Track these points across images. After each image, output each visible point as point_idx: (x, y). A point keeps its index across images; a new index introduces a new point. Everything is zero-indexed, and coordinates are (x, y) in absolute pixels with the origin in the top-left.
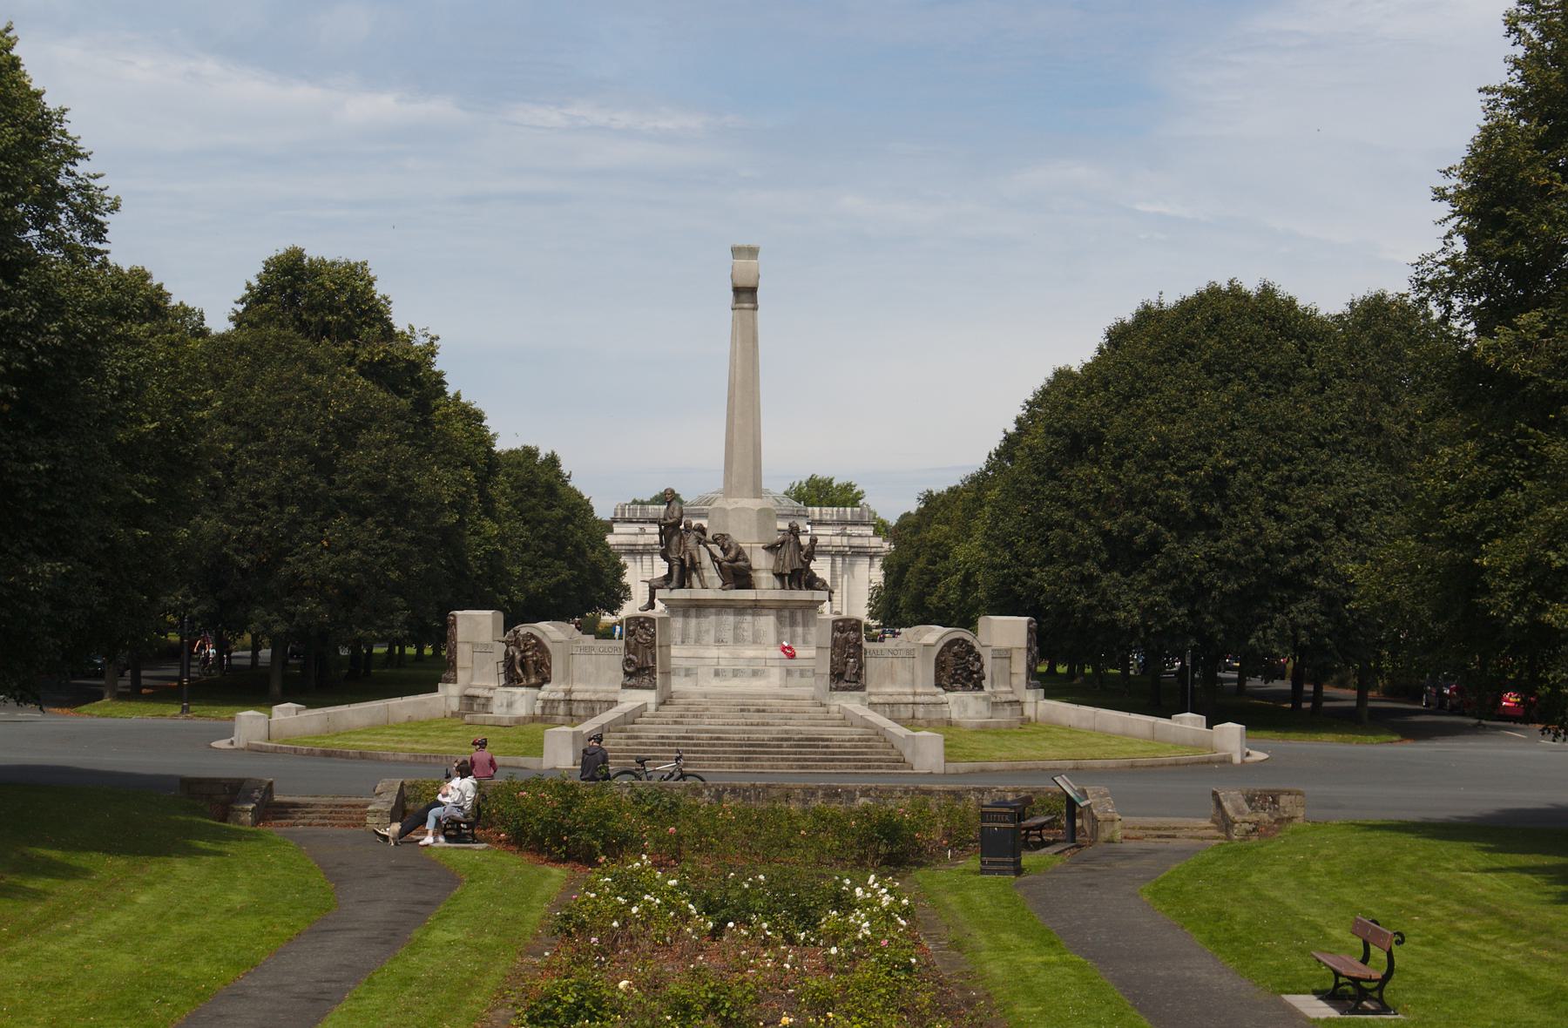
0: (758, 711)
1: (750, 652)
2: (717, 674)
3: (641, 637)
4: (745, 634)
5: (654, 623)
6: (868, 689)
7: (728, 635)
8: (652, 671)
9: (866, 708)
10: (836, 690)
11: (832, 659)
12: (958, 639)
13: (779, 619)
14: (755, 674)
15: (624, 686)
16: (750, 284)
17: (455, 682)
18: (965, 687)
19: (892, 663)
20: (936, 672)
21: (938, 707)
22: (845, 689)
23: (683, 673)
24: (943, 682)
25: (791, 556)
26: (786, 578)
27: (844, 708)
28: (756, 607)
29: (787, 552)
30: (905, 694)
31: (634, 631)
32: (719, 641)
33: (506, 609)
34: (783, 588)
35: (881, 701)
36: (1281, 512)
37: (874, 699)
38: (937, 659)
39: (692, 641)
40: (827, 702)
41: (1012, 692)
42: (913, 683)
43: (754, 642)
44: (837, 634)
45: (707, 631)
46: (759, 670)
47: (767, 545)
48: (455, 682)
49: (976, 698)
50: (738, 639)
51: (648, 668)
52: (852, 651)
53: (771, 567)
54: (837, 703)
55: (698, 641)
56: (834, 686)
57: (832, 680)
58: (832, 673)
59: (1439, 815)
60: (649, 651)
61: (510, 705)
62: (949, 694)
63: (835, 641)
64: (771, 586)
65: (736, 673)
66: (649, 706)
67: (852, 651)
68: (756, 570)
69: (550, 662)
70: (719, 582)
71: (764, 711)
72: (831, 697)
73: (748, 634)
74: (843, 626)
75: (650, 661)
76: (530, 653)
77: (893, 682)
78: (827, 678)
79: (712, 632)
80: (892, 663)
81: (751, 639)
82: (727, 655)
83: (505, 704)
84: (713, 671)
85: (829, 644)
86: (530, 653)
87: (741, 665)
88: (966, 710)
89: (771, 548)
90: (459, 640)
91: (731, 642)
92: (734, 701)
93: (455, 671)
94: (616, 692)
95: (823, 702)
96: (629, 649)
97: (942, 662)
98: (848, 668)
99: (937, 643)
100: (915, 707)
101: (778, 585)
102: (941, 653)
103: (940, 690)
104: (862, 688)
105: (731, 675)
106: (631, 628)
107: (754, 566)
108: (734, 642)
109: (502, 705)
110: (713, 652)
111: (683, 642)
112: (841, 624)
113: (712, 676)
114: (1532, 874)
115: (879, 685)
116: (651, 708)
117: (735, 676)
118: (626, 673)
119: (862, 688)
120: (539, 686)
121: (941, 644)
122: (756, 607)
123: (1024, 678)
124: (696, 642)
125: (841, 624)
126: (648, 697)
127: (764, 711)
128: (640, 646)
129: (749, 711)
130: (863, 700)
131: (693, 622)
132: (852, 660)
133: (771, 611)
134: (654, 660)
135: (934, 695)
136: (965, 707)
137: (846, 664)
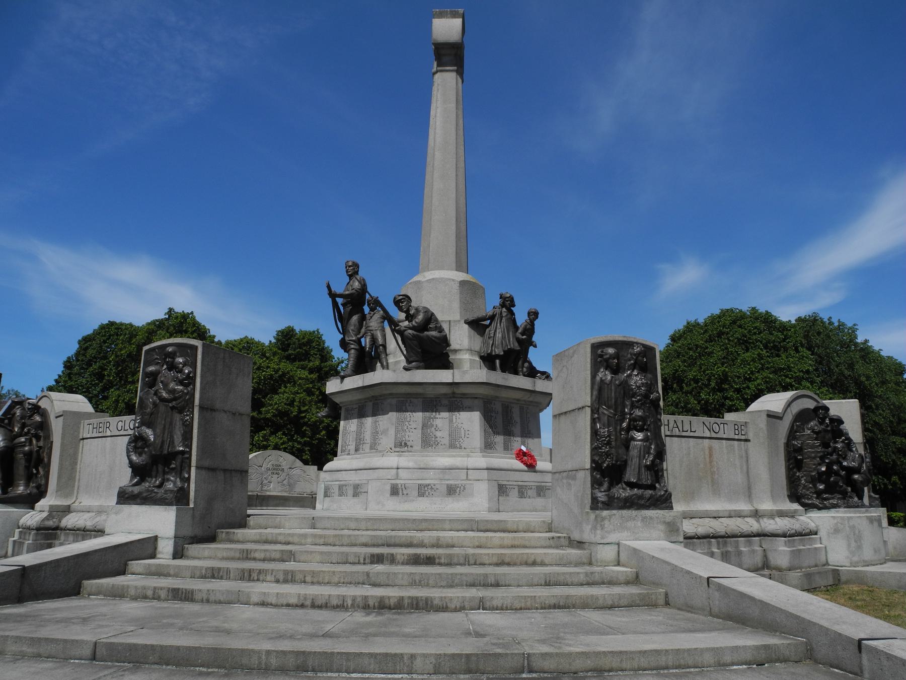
0: (416, 560)
1: (444, 460)
3: (166, 385)
4: (438, 434)
6: (679, 507)
7: (414, 436)
9: (680, 548)
10: (609, 504)
11: (595, 433)
13: (488, 417)
14: (451, 491)
15: (125, 497)
19: (710, 449)
20: (789, 470)
22: (628, 504)
23: (350, 491)
24: (801, 491)
25: (503, 333)
26: (498, 362)
27: (635, 551)
29: (499, 331)
30: (739, 515)
32: (401, 445)
35: (701, 531)
37: (689, 527)
38: (788, 445)
39: (367, 447)
40: (587, 536)
42: (749, 493)
43: (452, 446)
44: (606, 375)
45: (385, 432)
46: (457, 486)
47: (471, 319)
50: (428, 442)
51: (174, 455)
52: (638, 413)
54: (613, 537)
55: (373, 447)
56: (601, 496)
57: (596, 483)
58: (596, 467)
60: (177, 417)
62: (815, 515)
63: (600, 391)
65: (423, 491)
67: (638, 413)
68: (456, 351)
70: (403, 362)
71: (430, 561)
72: (599, 523)
73: (443, 435)
74: (617, 356)
77: (716, 490)
78: (584, 478)
79: (392, 432)
80: (710, 449)
81: (446, 441)
82: (411, 465)
84: (388, 487)
85: (586, 398)
86: (23, 439)
87: (431, 478)
88: (859, 547)
89: (477, 325)
91: (418, 445)
92: (365, 535)
94: (100, 511)
95: (576, 536)
98: (634, 452)
100: (767, 543)
103: (796, 506)
104: (664, 502)
105: (416, 493)
106: (151, 368)
110: (392, 460)
111: (357, 450)
112: (611, 351)
113: (388, 494)
115: (691, 496)
117: (421, 494)
119: (664, 502)
124: (371, 448)
125: (611, 351)
127: (430, 561)
128: (162, 408)
129: (392, 560)
130: (672, 529)
131: (369, 421)
132: (639, 436)
133: (476, 401)
134: (187, 438)
135: (792, 515)
137: (627, 444)
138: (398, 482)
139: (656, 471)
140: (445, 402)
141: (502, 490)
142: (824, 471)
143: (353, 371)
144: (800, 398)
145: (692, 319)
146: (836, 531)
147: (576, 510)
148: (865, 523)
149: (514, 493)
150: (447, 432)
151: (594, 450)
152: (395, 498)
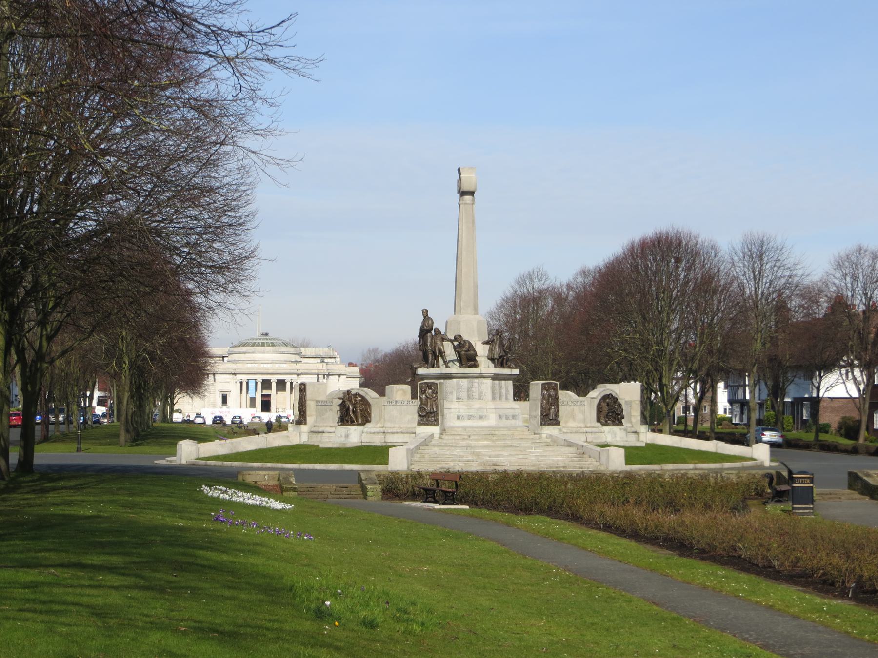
2: (458, 418)
4: (474, 394)
5: (437, 386)
8: (436, 414)
10: (545, 425)
12: (608, 395)
14: (481, 417)
15: (419, 424)
16: (472, 190)
17: (305, 424)
18: (614, 424)
19: (573, 409)
21: (320, 435)
28: (481, 376)
31: (425, 391)
33: (171, 400)
34: (495, 367)
36: (864, 308)
40: (539, 432)
41: (632, 427)
43: (479, 399)
46: (483, 416)
48: (305, 424)
49: (621, 429)
53: (487, 355)
56: (543, 423)
59: (207, 456)
60: (434, 402)
61: (347, 436)
64: (486, 366)
65: (470, 417)
66: (435, 435)
69: (371, 411)
75: (434, 409)
76: (670, 391)
79: (455, 393)
83: (343, 436)
87: (472, 412)
88: (615, 437)
90: (307, 399)
91: (465, 399)
93: (305, 417)
94: (415, 428)
95: (536, 432)
96: (421, 402)
97: (601, 408)
99: (597, 397)
101: (493, 365)
102: (599, 404)
103: (599, 424)
107: (478, 354)
108: (468, 399)
109: (341, 436)
114: (252, 467)
116: (436, 436)
117: (469, 419)
118: (420, 416)
120: (363, 424)
121: (600, 397)
122: (481, 376)
123: (639, 418)
126: (434, 430)
134: (437, 408)
136: (615, 434)
138: (460, 414)
139: (557, 415)
140: (713, 407)
141: (500, 417)
142: (814, 397)
143: (385, 360)
144: (818, 411)
145: (629, 383)
146: (609, 432)
147: (536, 425)
148: (618, 430)
149: (504, 418)
150: (477, 393)
151: (542, 411)
152: (458, 420)
